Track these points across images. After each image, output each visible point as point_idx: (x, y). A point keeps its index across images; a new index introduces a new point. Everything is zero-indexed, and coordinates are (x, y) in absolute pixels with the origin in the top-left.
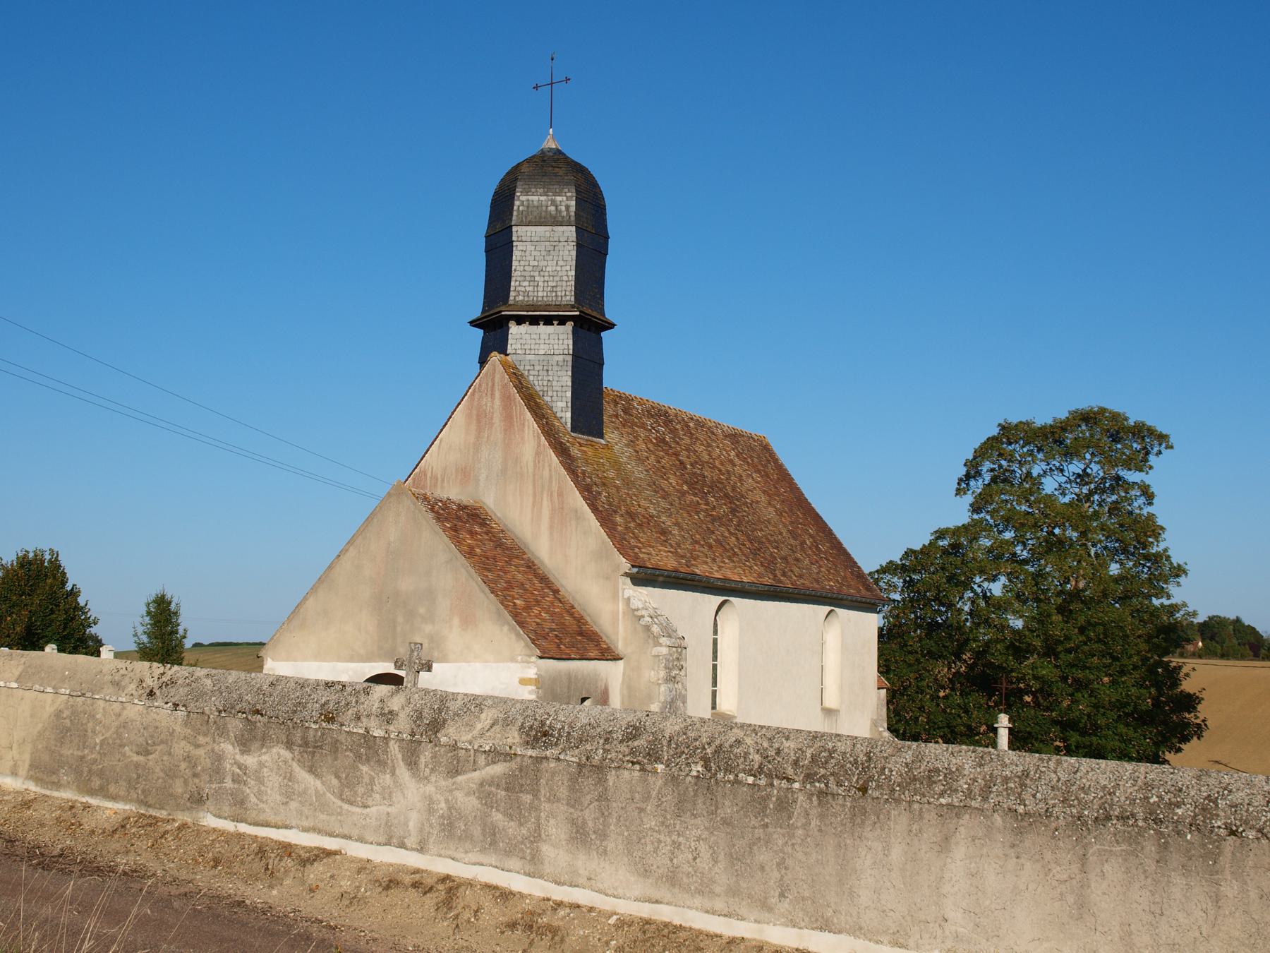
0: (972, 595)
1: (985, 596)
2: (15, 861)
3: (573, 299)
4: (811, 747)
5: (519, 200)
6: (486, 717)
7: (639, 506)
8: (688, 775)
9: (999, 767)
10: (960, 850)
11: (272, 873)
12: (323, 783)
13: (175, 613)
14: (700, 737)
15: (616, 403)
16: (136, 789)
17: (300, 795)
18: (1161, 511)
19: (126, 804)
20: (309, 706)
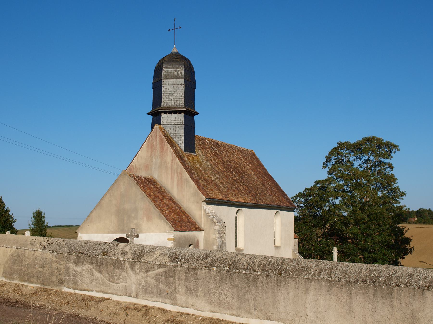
0: (329, 204)
1: (333, 205)
2: (1, 304)
3: (184, 105)
4: (264, 261)
5: (164, 70)
6: (157, 253)
7: (208, 177)
8: (224, 271)
9: (324, 266)
10: (312, 293)
11: (87, 306)
12: (103, 276)
13: (44, 217)
14: (227, 258)
15: (200, 140)
16: (40, 279)
17: (96, 280)
18: (396, 173)
19: (37, 284)
20: (98, 250)
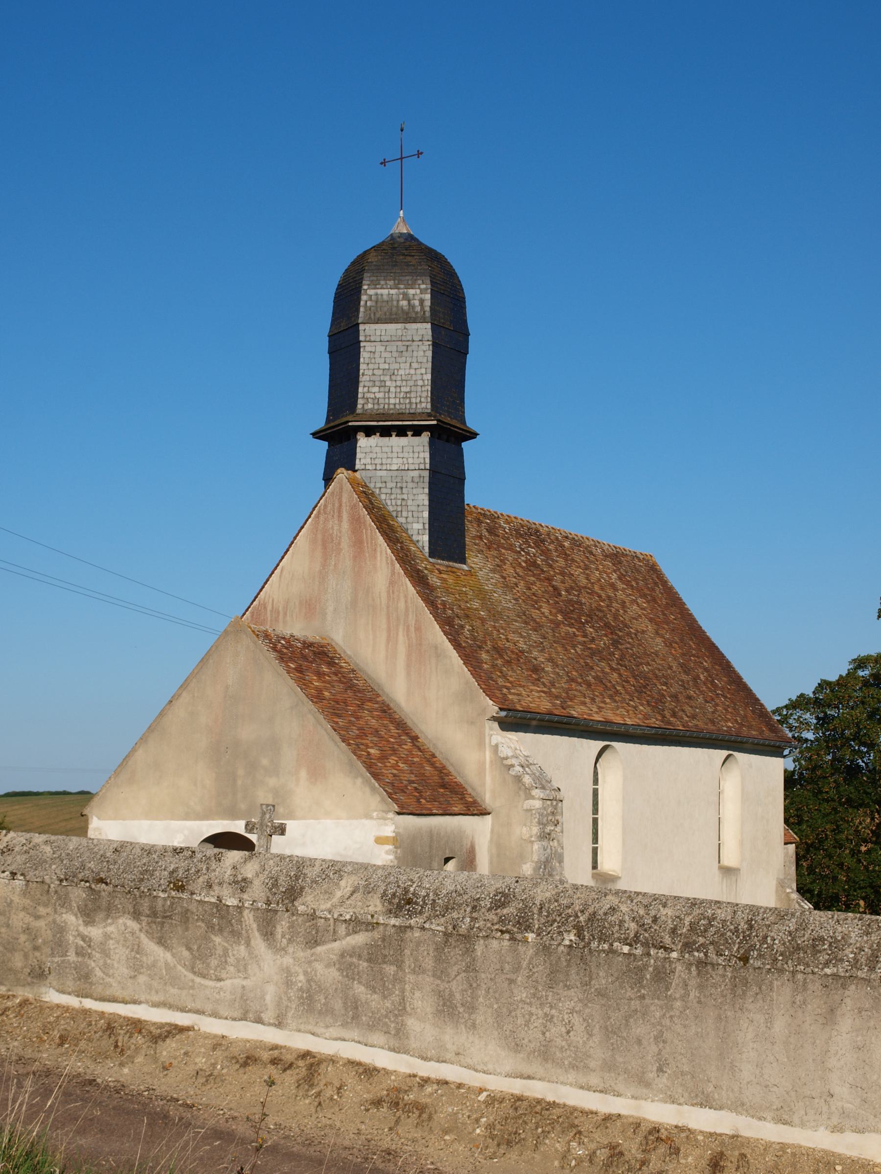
3: (429, 406)
4: (690, 914)
6: (346, 884)
10: (846, 1023)
11: (122, 1050)
12: (173, 955)
15: (479, 522)
17: (149, 968)
20: (157, 873)
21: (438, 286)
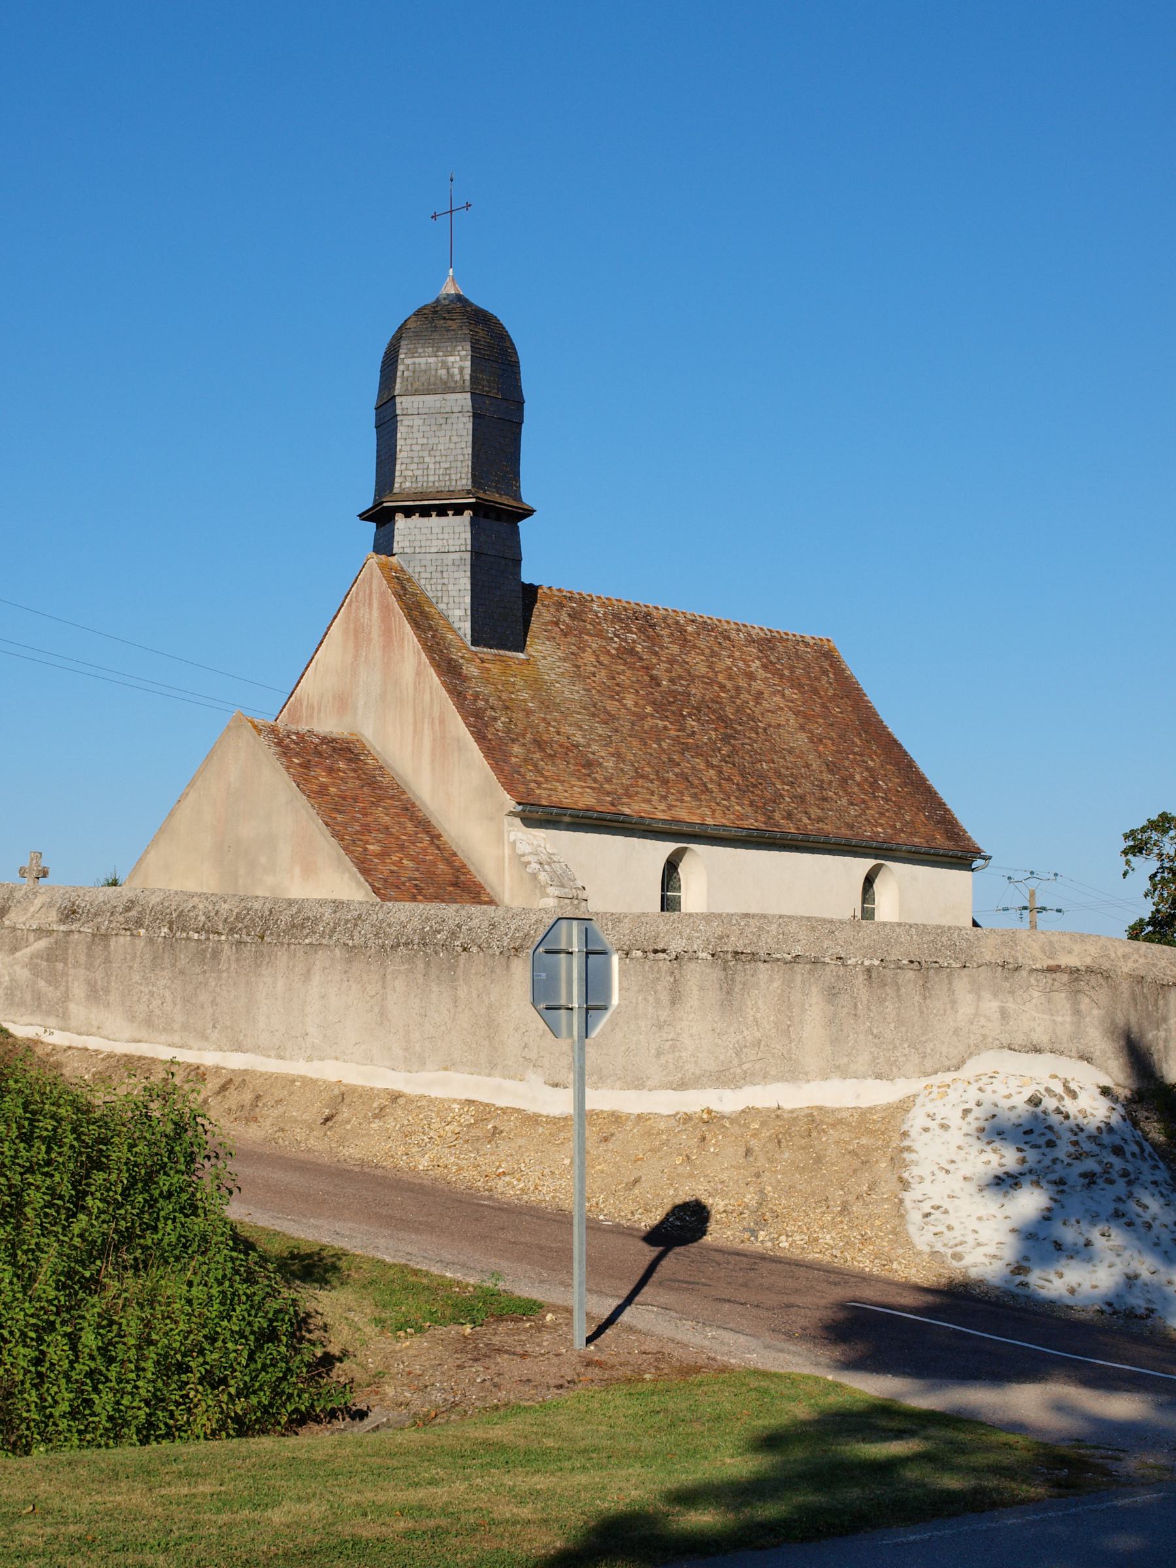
3: (470, 482)
10: (316, 979)
15: (560, 606)
21: (482, 352)
